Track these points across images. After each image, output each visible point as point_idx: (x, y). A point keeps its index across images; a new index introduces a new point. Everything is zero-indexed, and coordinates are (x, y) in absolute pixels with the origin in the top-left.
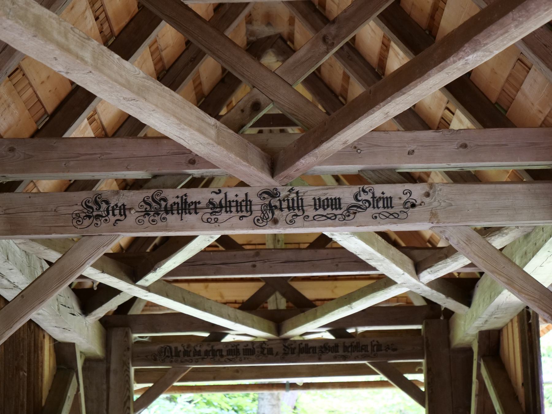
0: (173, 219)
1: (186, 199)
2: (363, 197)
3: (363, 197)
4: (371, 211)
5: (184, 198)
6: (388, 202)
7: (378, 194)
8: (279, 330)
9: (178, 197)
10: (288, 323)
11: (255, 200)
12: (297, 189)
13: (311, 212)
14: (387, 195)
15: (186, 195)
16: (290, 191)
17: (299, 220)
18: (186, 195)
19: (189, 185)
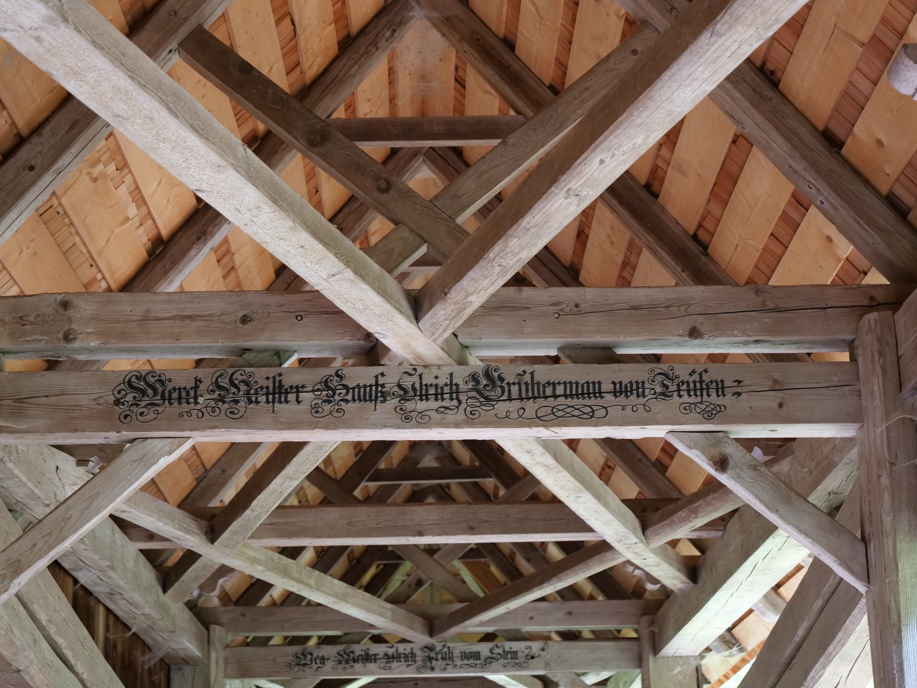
2: (496, 651)
3: (496, 651)
4: (502, 661)
6: (514, 654)
11: (418, 653)
13: (458, 662)
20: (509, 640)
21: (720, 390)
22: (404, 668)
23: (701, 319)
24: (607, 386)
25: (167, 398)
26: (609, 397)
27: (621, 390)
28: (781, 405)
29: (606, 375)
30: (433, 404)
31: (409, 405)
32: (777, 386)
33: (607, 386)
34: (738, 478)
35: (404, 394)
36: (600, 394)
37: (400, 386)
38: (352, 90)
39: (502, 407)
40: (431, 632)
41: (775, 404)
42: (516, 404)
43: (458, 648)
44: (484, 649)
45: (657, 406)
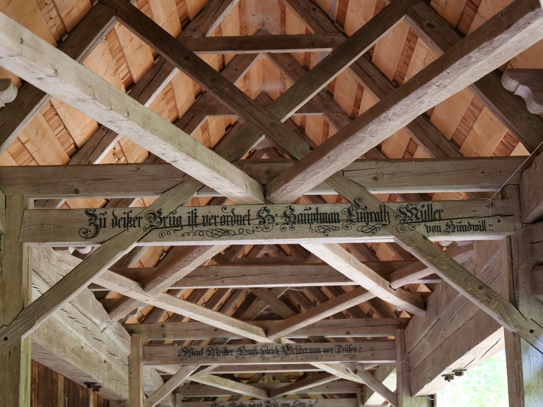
1: (195, 213)
2: (296, 403)
3: (296, 403)
7: (301, 402)
9: (223, 348)
11: (263, 404)
12: (276, 400)
14: (304, 402)
16: (274, 401)
19: (229, 343)
23: (350, 329)
24: (322, 350)
25: (193, 354)
26: (323, 353)
27: (326, 351)
29: (322, 346)
30: (271, 355)
31: (264, 356)
32: (372, 349)
33: (322, 350)
35: (263, 352)
36: (319, 352)
37: (262, 350)
39: (291, 356)
40: (269, 395)
41: (371, 355)
42: (295, 355)
45: (337, 355)
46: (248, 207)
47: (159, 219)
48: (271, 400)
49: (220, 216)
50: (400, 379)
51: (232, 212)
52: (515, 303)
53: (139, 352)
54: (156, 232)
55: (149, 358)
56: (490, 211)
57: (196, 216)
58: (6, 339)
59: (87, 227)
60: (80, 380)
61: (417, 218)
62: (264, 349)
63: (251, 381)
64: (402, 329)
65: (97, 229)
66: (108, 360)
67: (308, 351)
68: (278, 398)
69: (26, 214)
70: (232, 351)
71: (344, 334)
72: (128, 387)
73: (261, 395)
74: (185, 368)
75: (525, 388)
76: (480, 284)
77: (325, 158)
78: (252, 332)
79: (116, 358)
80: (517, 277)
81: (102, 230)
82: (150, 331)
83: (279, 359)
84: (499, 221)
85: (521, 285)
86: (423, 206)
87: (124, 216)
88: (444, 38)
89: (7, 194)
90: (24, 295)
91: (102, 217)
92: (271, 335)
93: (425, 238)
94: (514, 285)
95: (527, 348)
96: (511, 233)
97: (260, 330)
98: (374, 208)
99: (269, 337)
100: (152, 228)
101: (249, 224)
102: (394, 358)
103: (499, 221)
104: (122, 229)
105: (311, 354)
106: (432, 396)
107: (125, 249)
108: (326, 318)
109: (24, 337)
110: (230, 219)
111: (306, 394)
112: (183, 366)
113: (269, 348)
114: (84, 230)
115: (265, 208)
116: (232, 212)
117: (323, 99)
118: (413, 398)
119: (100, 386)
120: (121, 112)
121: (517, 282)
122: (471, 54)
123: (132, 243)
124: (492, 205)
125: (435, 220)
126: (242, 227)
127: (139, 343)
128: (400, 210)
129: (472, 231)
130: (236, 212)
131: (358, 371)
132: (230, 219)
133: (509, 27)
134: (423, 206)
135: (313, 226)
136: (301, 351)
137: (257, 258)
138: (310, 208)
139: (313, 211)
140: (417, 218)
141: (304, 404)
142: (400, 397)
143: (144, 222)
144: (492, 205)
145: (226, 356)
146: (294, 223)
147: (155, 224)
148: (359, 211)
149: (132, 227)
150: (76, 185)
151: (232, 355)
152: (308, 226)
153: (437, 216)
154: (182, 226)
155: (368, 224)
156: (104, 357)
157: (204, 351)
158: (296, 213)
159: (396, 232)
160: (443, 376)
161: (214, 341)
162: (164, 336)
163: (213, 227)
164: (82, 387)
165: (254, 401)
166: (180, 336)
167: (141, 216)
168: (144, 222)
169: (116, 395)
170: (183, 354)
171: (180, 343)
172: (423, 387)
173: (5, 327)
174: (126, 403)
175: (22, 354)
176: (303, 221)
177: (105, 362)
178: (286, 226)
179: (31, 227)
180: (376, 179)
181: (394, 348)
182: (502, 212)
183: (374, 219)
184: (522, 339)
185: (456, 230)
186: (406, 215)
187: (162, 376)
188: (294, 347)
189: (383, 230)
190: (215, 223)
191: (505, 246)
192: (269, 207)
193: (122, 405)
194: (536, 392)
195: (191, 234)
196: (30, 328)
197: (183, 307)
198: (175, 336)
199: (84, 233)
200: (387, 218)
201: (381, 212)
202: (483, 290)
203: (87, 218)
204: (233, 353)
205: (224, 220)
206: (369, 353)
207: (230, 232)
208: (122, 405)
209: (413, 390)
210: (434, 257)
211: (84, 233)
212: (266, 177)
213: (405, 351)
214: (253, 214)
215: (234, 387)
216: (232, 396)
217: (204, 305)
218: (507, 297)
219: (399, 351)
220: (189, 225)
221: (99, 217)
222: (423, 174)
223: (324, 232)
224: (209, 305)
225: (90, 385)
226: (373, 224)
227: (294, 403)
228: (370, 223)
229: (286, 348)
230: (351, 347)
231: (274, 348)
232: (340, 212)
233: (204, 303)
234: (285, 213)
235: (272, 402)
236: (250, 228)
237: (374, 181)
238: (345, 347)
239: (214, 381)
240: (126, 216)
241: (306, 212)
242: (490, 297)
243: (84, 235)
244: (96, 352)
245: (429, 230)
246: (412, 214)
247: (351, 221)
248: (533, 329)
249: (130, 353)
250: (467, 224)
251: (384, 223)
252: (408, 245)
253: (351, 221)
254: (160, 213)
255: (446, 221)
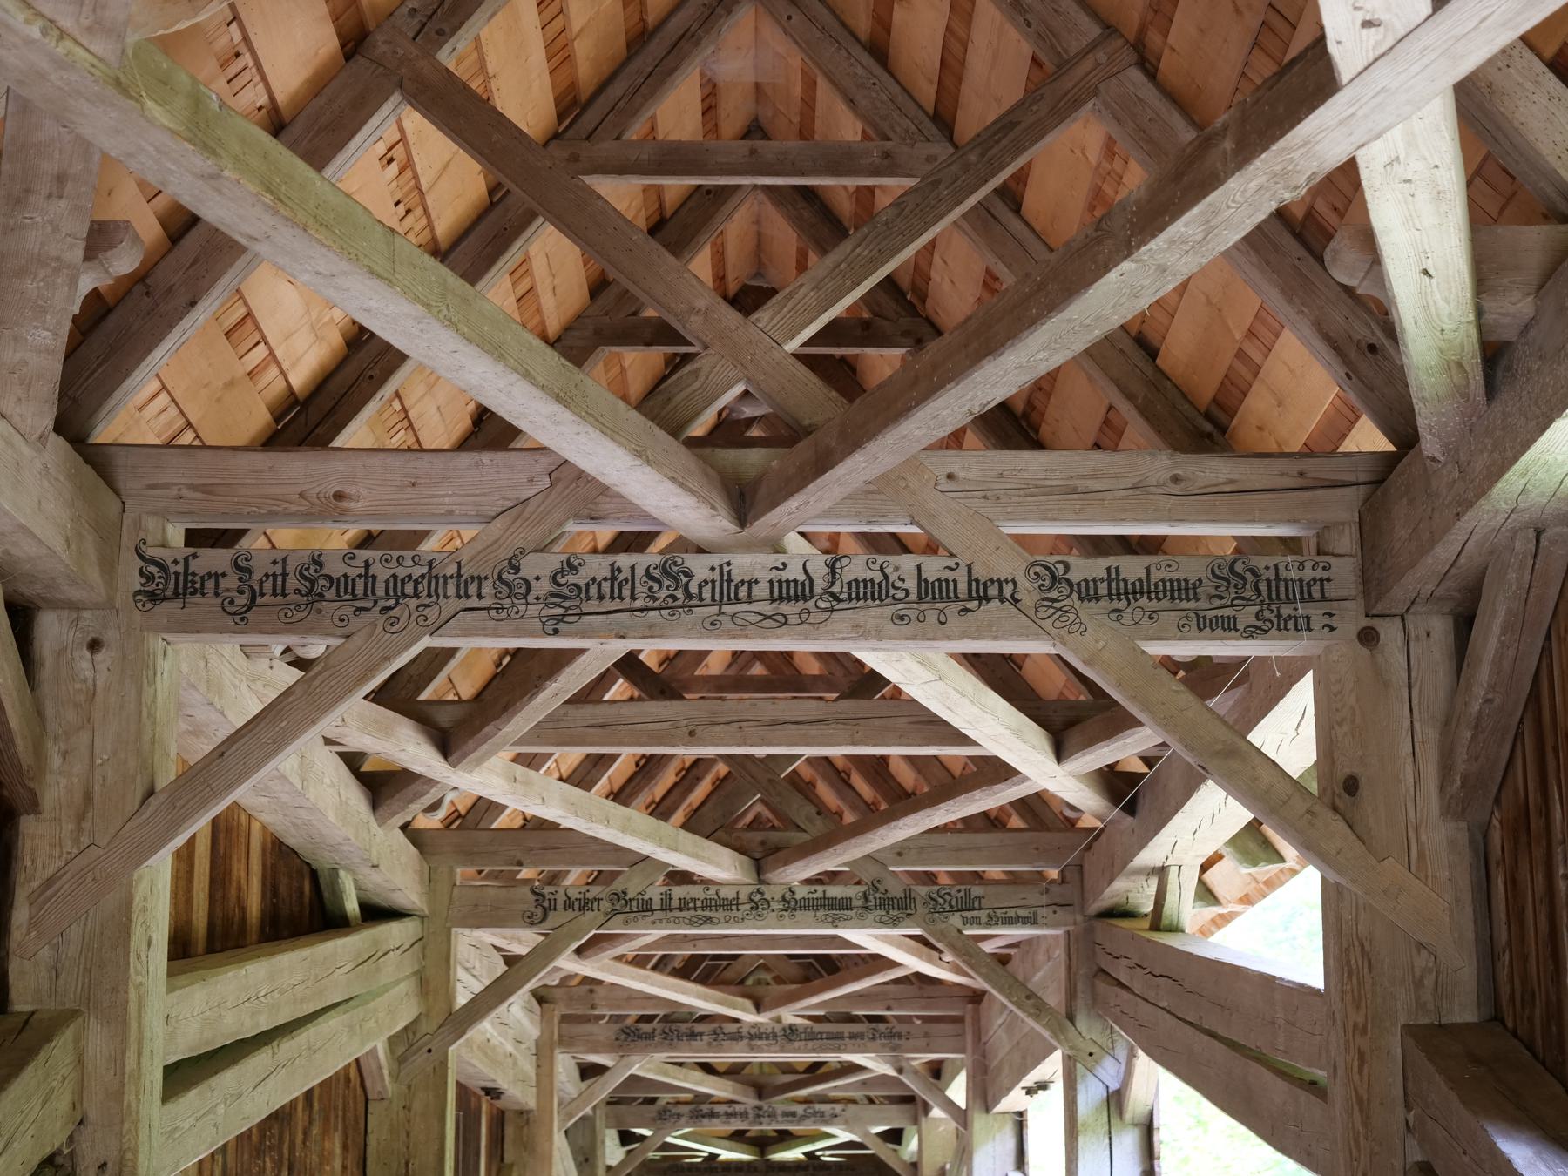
0: (705, 1121)
2: (809, 1111)
3: (809, 1111)
4: (813, 1119)
5: (726, 568)
6: (822, 1114)
8: (762, 1153)
10: (770, 1148)
11: (750, 1111)
13: (780, 1119)
15: (729, 564)
17: (774, 1123)
18: (729, 564)
20: (820, 1102)
21: (1168, 588)
22: (739, 1123)
23: (892, 1001)
24: (846, 1035)
25: (640, 1037)
26: (847, 1040)
27: (853, 1036)
28: (928, 1045)
29: (847, 1028)
30: (765, 1042)
31: (754, 1043)
32: (926, 1035)
33: (846, 1035)
34: (908, 1078)
35: (751, 1037)
36: (842, 1038)
37: (749, 1034)
38: (650, 113)
39: (797, 1044)
40: (760, 1096)
41: (925, 1044)
42: (804, 1042)
43: (780, 1108)
44: (800, 1109)
45: (870, 1044)
46: (736, 889)
47: (623, 902)
48: (764, 1105)
49: (702, 898)
50: (971, 1085)
51: (717, 894)
52: (1071, 1018)
53: (553, 1033)
54: (619, 918)
55: (566, 1042)
56: (1044, 899)
57: (671, 899)
58: (430, 1051)
59: (533, 909)
60: (475, 1085)
61: (951, 907)
62: (753, 1031)
63: (733, 1072)
64: (976, 1005)
65: (546, 911)
66: (514, 1052)
67: (824, 1036)
68: (776, 1103)
69: (456, 891)
70: (701, 1034)
71: (882, 1010)
72: (534, 1090)
73: (747, 1096)
74: (625, 1059)
75: (1079, 1125)
76: (1028, 993)
77: (831, 850)
78: (734, 1008)
79: (523, 1046)
80: (1075, 985)
81: (551, 914)
82: (571, 998)
83: (777, 1048)
84: (1055, 912)
85: (1080, 995)
86: (959, 891)
87: (579, 896)
88: (993, 671)
89: (432, 866)
90: (450, 998)
91: (552, 897)
92: (765, 1011)
93: (960, 931)
94: (1071, 995)
95: (1084, 1076)
96: (1071, 928)
97: (748, 1003)
98: (896, 891)
99: (763, 1014)
100: (615, 912)
101: (738, 910)
102: (963, 1051)
103: (1055, 912)
104: (577, 913)
105: (829, 1042)
106: (1021, 1114)
107: (580, 939)
108: (936, 829)
109: (451, 1049)
110: (713, 902)
111: (825, 1096)
112: (622, 1056)
113: (762, 1031)
114: (529, 914)
115: (758, 890)
116: (717, 894)
117: (849, 672)
118: (990, 1117)
119: (502, 1093)
120: (601, 822)
121: (1075, 991)
122: (975, 793)
123: (591, 930)
124: (1047, 891)
125: (974, 909)
126: (729, 913)
127: (553, 1019)
128: (930, 896)
129: (1020, 924)
130: (722, 895)
131: (905, 1070)
132: (713, 902)
133: (1006, 780)
134: (959, 891)
135: (818, 914)
136: (811, 1036)
137: (752, 676)
138: (816, 891)
139: (819, 895)
140: (951, 907)
141: (823, 1112)
142: (969, 1113)
143: (605, 905)
144: (1047, 891)
145: (693, 1043)
146: (795, 909)
147: (618, 907)
148: (878, 895)
149: (590, 912)
150: (519, 855)
151: (701, 1040)
152: (812, 913)
153: (976, 905)
154: (653, 911)
155: (888, 913)
156: (510, 1048)
157: (657, 1032)
158: (798, 897)
159: (924, 924)
160: (1023, 1088)
161: (673, 1017)
162: (593, 1007)
163: (692, 913)
164: (475, 1094)
165: (734, 1105)
166: (619, 1007)
167: (600, 896)
168: (605, 905)
169: (519, 1103)
170: (623, 1036)
171: (620, 1018)
172: (999, 1102)
173: (429, 1036)
174: (531, 1115)
175: (449, 1071)
176: (807, 908)
177: (511, 1055)
178: (784, 913)
179: (462, 909)
180: (900, 854)
181: (962, 1034)
182: (1057, 900)
183: (896, 906)
184: (1078, 1065)
185: (1000, 922)
186: (936, 901)
187: (578, 1064)
188: (801, 1030)
189: (907, 920)
190: (695, 907)
191: (1062, 942)
192: (763, 888)
193: (525, 1117)
194: (1094, 1131)
195: (664, 921)
196: (460, 1037)
197: (633, 978)
198: (611, 1007)
199: (529, 917)
200: (913, 905)
201: (906, 898)
202: (1032, 1001)
203: (532, 897)
204: (704, 1037)
205: (707, 905)
206: (923, 1042)
207: (715, 920)
208: (525, 1117)
209: (989, 1104)
210: (971, 956)
211: (529, 917)
212: (760, 849)
213: (980, 1039)
214: (743, 898)
215: (699, 1083)
216: (696, 1096)
217: (612, 797)
218: (1063, 1011)
219: (969, 1038)
220: (662, 910)
221: (547, 897)
222: (959, 849)
223: (833, 922)
224: (620, 795)
225: (488, 1091)
226: (895, 912)
227: (805, 1110)
228: (891, 912)
229: (789, 1031)
230: (894, 1031)
231: (769, 1031)
232: (853, 896)
233: (612, 793)
234: (783, 897)
235: (765, 1107)
236: (739, 915)
237: (899, 858)
238: (883, 1030)
239: (666, 1074)
240: (582, 896)
241: (811, 896)
242: (1040, 1010)
243: (528, 920)
244: (501, 1043)
245: (966, 921)
246: (945, 901)
247: (867, 908)
248: (1093, 1051)
249: (539, 1034)
250: (1014, 915)
251: (909, 911)
252: (939, 941)
253: (867, 908)
254: (625, 893)
255: (988, 911)
